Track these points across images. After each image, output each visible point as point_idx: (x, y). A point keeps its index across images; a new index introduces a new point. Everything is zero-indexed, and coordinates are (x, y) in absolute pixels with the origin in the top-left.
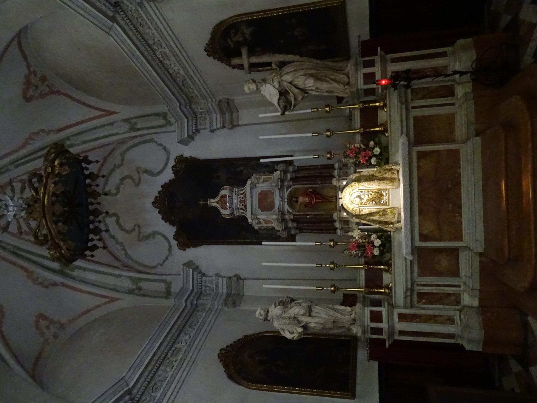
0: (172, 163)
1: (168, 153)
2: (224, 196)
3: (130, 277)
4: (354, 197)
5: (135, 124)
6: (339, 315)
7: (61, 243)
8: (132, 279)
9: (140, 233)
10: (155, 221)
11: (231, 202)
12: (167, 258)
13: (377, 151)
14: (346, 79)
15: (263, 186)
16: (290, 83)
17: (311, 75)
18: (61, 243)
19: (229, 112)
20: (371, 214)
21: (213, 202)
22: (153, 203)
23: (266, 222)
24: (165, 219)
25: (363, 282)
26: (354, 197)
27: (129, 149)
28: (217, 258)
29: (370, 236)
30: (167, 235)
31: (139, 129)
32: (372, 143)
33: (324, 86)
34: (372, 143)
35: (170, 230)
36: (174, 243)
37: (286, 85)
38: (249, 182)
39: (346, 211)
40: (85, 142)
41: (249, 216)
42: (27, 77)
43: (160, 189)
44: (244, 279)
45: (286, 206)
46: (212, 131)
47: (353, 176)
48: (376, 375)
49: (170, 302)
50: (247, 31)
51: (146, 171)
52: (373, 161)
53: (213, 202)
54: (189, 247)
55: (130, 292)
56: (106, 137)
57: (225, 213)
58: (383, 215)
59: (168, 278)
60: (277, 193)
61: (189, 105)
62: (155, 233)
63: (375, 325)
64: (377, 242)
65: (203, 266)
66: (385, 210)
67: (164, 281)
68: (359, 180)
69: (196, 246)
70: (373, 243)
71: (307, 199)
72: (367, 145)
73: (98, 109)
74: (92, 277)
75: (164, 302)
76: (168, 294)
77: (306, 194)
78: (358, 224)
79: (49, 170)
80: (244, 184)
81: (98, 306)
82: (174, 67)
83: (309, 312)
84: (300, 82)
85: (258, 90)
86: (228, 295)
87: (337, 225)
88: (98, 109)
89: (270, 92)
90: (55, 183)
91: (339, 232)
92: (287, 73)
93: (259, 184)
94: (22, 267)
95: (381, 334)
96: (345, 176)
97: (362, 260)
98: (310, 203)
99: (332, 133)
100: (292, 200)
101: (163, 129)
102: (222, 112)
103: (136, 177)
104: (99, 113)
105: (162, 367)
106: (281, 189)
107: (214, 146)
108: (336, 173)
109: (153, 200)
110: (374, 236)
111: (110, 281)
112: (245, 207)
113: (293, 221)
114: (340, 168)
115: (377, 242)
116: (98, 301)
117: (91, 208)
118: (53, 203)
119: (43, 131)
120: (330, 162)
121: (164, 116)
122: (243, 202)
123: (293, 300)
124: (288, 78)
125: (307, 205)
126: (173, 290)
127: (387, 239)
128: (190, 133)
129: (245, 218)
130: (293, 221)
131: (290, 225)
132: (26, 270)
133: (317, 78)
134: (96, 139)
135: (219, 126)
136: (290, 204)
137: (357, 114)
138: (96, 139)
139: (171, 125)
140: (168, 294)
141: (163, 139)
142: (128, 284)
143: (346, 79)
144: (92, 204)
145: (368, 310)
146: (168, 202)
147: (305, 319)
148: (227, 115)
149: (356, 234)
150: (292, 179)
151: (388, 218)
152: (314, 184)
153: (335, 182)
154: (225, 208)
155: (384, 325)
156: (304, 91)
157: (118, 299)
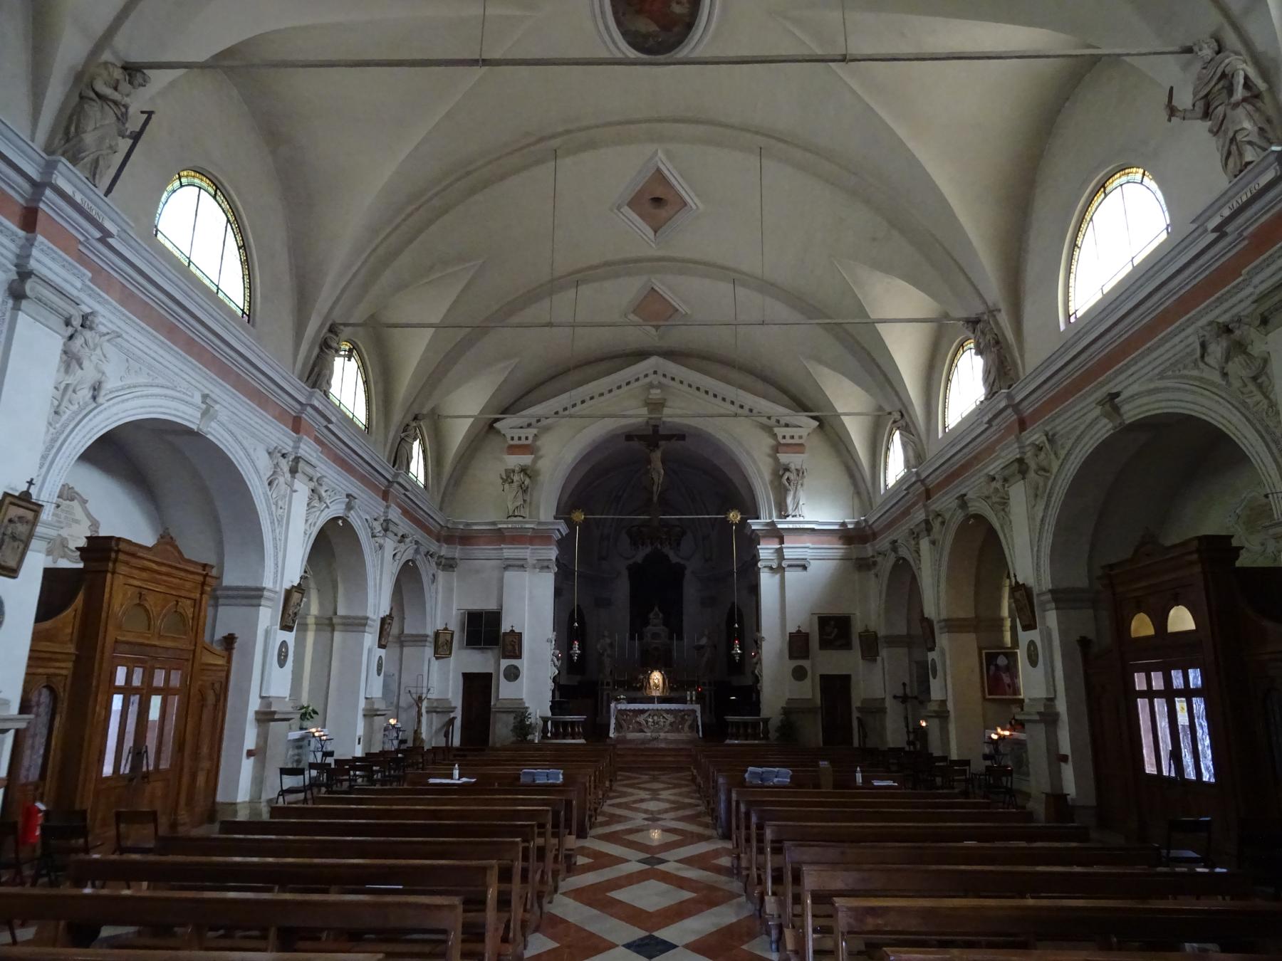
4: (656, 677)
21: (656, 609)
28: (622, 590)
36: (631, 562)
41: (649, 627)
53: (656, 609)
57: (651, 616)
89: (704, 641)
107: (691, 591)
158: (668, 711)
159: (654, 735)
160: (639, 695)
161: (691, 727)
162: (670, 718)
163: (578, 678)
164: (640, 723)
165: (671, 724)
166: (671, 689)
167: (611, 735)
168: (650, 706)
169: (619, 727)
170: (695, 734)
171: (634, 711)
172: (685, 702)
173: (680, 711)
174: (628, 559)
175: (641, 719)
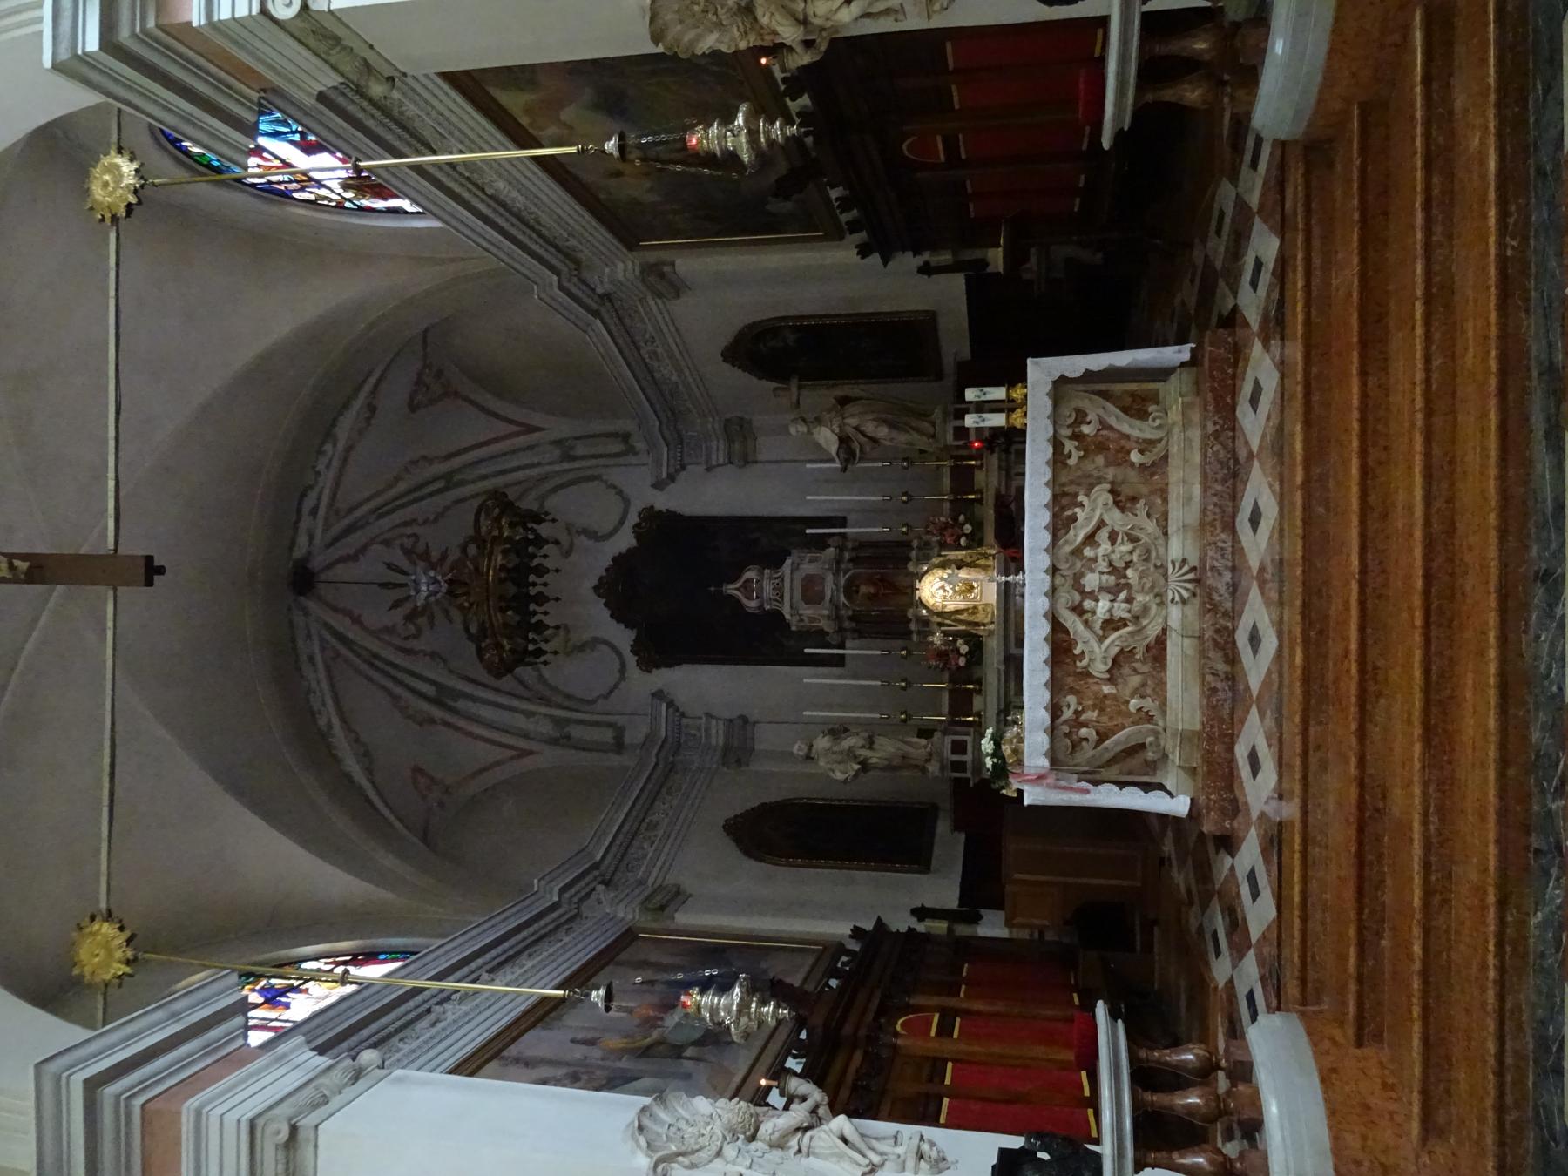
0: (633, 519)
1: (627, 502)
2: (750, 581)
3: (551, 716)
4: (935, 590)
5: (572, 448)
6: (910, 750)
7: (505, 642)
8: (557, 722)
9: (567, 641)
10: (598, 620)
11: (761, 590)
12: (616, 686)
13: (968, 528)
14: (931, 430)
15: (808, 568)
16: (856, 428)
17: (885, 421)
18: (505, 642)
19: (740, 441)
20: (957, 612)
21: (731, 589)
22: (596, 589)
23: (812, 620)
24: (617, 616)
25: (945, 709)
26: (935, 590)
27: (554, 490)
28: (707, 687)
29: (955, 641)
30: (616, 643)
31: (575, 458)
32: (962, 518)
33: (903, 438)
34: (962, 518)
35: (623, 637)
36: (631, 660)
37: (850, 431)
38: (788, 562)
39: (925, 607)
40: (484, 477)
41: (786, 611)
42: (420, 374)
43: (608, 562)
44: (755, 723)
45: (843, 599)
46: (709, 469)
47: (936, 561)
48: (961, 848)
49: (627, 760)
50: (791, 338)
51: (586, 532)
52: (963, 541)
53: (731, 589)
54: (658, 667)
55: (554, 742)
56: (519, 468)
57: (752, 605)
58: (973, 613)
59: (621, 720)
60: (830, 578)
61: (674, 421)
62: (596, 642)
63: (955, 758)
64: (964, 649)
65: (682, 697)
66: (975, 607)
67: (610, 725)
68: (943, 566)
69: (670, 665)
70: (958, 650)
71: (872, 590)
72: (955, 519)
73: (510, 421)
74: (486, 712)
75: (615, 760)
76: (619, 746)
77: (870, 581)
78: (940, 625)
79: (496, 533)
80: (777, 564)
81: (498, 763)
82: (665, 370)
83: (870, 743)
84: (870, 428)
85: (809, 432)
86: (727, 749)
87: (913, 626)
88: (510, 421)
89: (827, 437)
90: (504, 552)
91: (915, 637)
92: (852, 416)
93: (799, 567)
94: (383, 688)
95: (965, 771)
96: (925, 559)
97: (946, 676)
98: (875, 595)
99: (909, 684)
100: (850, 589)
101: (621, 460)
102: (730, 440)
103: (564, 539)
104: (514, 428)
105: (635, 843)
106: (836, 574)
107: (712, 494)
108: (913, 554)
109: (595, 582)
110: (960, 642)
111: (521, 722)
112: (782, 597)
113: (851, 619)
114: (919, 548)
115: (964, 649)
116: (498, 754)
117: (533, 591)
118: (502, 581)
119: (424, 458)
120: (905, 538)
121: (626, 437)
122: (779, 590)
123: (846, 730)
124: (853, 421)
125: (871, 597)
126: (627, 740)
127: (976, 644)
128: (672, 470)
129: (778, 615)
130: (851, 619)
131: (847, 624)
132: (390, 693)
133: (892, 425)
134: (504, 472)
135: (721, 461)
136: (848, 596)
137: (947, 473)
138: (504, 472)
139: (636, 454)
140: (619, 746)
141: (616, 476)
142: (546, 728)
143: (931, 430)
144: (534, 584)
145: (948, 740)
146: (623, 589)
147: (864, 753)
148: (737, 446)
149: (937, 639)
150: (851, 560)
151: (979, 618)
152: (1014, 664)
153: (911, 567)
154: (750, 598)
155: (968, 758)
156: (874, 440)
157: (531, 753)
158: (1060, 525)
159: (1177, 586)
160: (993, 649)
161: (1137, 408)
162: (1094, 508)
163: (943, 827)
164: (1119, 661)
165: (1123, 501)
166: (976, 540)
167: (1179, 806)
168: (1035, 607)
169: (1136, 765)
170: (1174, 392)
171: (1056, 686)
172: (1010, 442)
173: (1058, 459)
174: (623, 668)
175: (1095, 652)
